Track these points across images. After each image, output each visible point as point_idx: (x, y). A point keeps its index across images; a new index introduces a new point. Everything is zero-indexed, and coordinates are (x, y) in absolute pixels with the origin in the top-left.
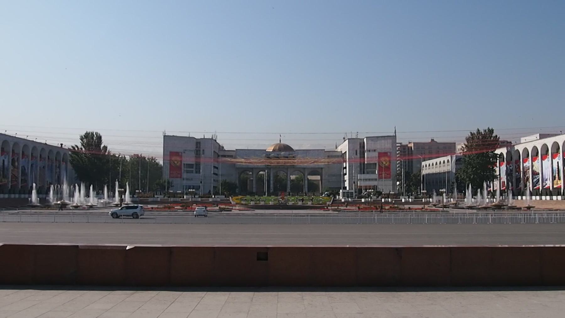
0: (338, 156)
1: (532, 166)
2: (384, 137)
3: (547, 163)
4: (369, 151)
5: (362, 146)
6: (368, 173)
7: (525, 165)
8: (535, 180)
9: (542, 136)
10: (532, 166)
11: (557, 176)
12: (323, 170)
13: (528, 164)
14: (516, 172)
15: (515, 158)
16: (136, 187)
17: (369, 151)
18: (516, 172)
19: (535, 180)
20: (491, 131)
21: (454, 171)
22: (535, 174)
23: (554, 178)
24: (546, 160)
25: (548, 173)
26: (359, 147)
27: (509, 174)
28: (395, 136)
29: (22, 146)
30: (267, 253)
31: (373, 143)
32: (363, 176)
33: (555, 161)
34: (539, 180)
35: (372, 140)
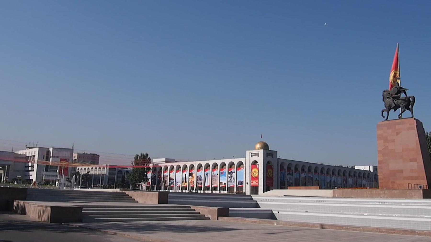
0: (23, 158)
1: (170, 175)
2: (61, 149)
3: (179, 174)
4: (54, 157)
5: (48, 152)
6: (51, 171)
7: (164, 174)
8: (170, 182)
9: (166, 162)
10: (170, 175)
11: (184, 181)
12: (10, 166)
13: (167, 173)
14: (158, 177)
15: (158, 170)
17: (54, 157)
18: (158, 177)
19: (170, 182)
20: (147, 155)
21: (108, 174)
22: (170, 179)
23: (183, 182)
25: (179, 179)
26: (46, 154)
27: (153, 178)
28: (73, 149)
29: (358, 172)
30: (378, 188)
31: (57, 152)
32: (48, 173)
33: (184, 174)
34: (173, 182)
35: (57, 150)
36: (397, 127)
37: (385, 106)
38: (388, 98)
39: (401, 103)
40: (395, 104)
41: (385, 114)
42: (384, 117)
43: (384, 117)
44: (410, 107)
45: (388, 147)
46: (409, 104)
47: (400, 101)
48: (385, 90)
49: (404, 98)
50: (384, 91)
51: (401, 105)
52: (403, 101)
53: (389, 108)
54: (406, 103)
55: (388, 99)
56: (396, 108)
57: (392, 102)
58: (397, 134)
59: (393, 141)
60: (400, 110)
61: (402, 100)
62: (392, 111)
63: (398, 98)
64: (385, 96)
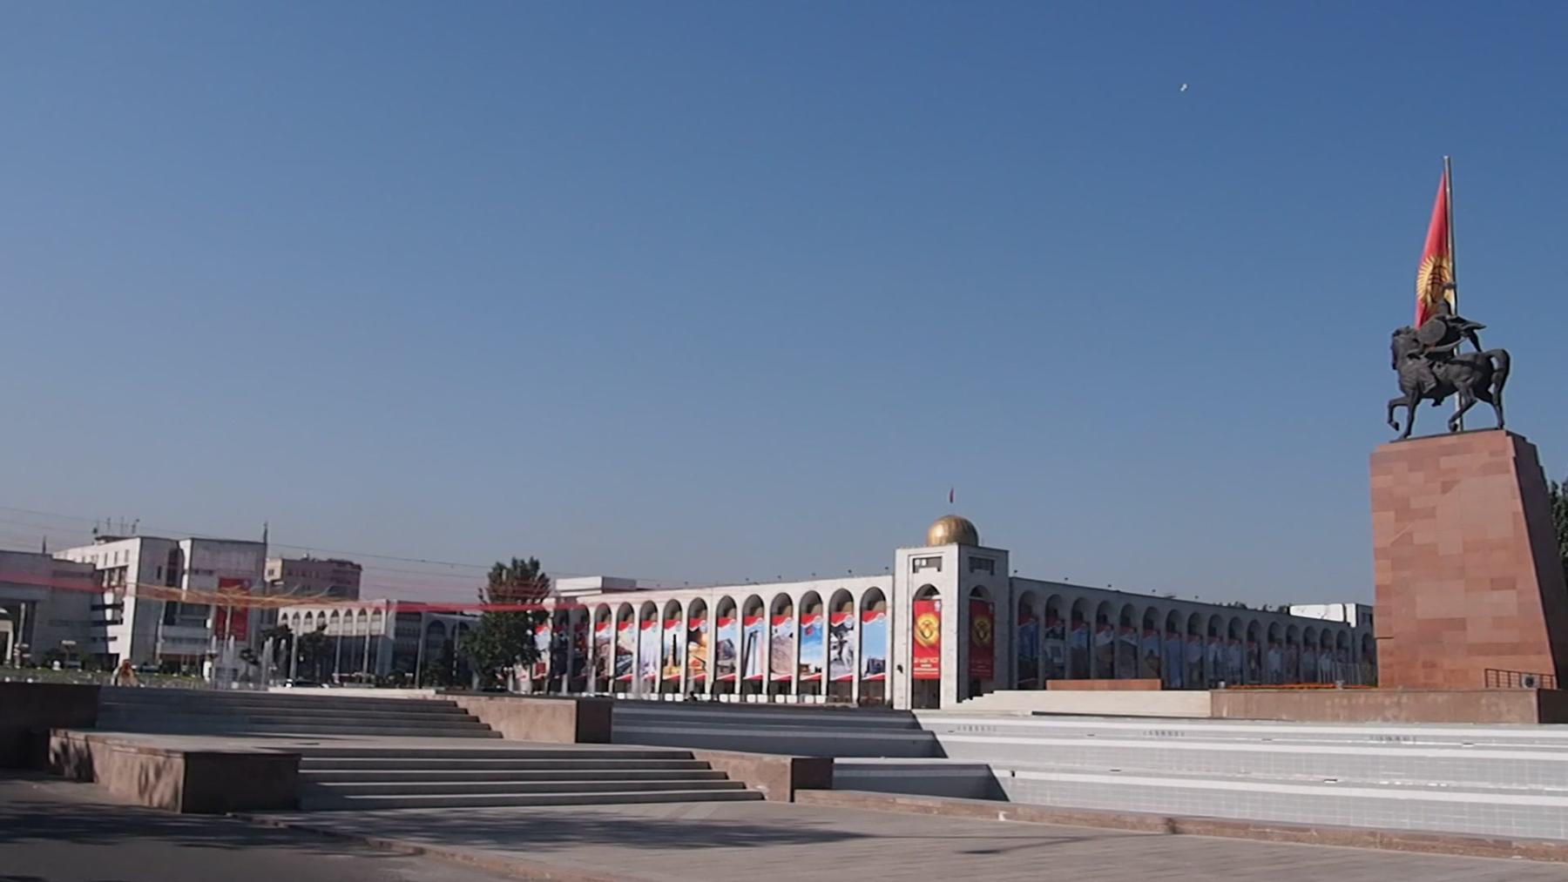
0: (82, 575)
1: (617, 638)
2: (221, 542)
3: (652, 636)
4: (197, 572)
5: (176, 554)
6: (184, 623)
7: (598, 634)
8: (620, 664)
9: (605, 589)
10: (617, 638)
11: (670, 658)
12: (38, 607)
13: (608, 632)
14: (576, 646)
15: (574, 619)
16: (68, 663)
17: (197, 572)
18: (576, 646)
19: (620, 664)
20: (535, 565)
21: (392, 636)
22: (619, 652)
23: (664, 663)
24: (727, 627)
25: (651, 652)
26: (166, 560)
27: (557, 649)
28: (265, 544)
31: (207, 554)
32: (173, 631)
33: (669, 634)
34: (629, 665)
35: (206, 548)
36: (1445, 462)
37: (1402, 388)
38: (1411, 356)
39: (1458, 375)
40: (1438, 380)
41: (1401, 414)
42: (1397, 427)
43: (1397, 427)
44: (1492, 389)
45: (1410, 534)
46: (1486, 379)
47: (1456, 368)
48: (1402, 326)
49: (1468, 359)
50: (1398, 333)
51: (1458, 383)
52: (1466, 368)
53: (1415, 394)
54: (1478, 375)
55: (1410, 362)
56: (1439, 393)
57: (1426, 371)
58: (1446, 488)
59: (1431, 513)
60: (1454, 401)
61: (1463, 363)
62: (1427, 403)
63: (1447, 358)
64: (1401, 351)
